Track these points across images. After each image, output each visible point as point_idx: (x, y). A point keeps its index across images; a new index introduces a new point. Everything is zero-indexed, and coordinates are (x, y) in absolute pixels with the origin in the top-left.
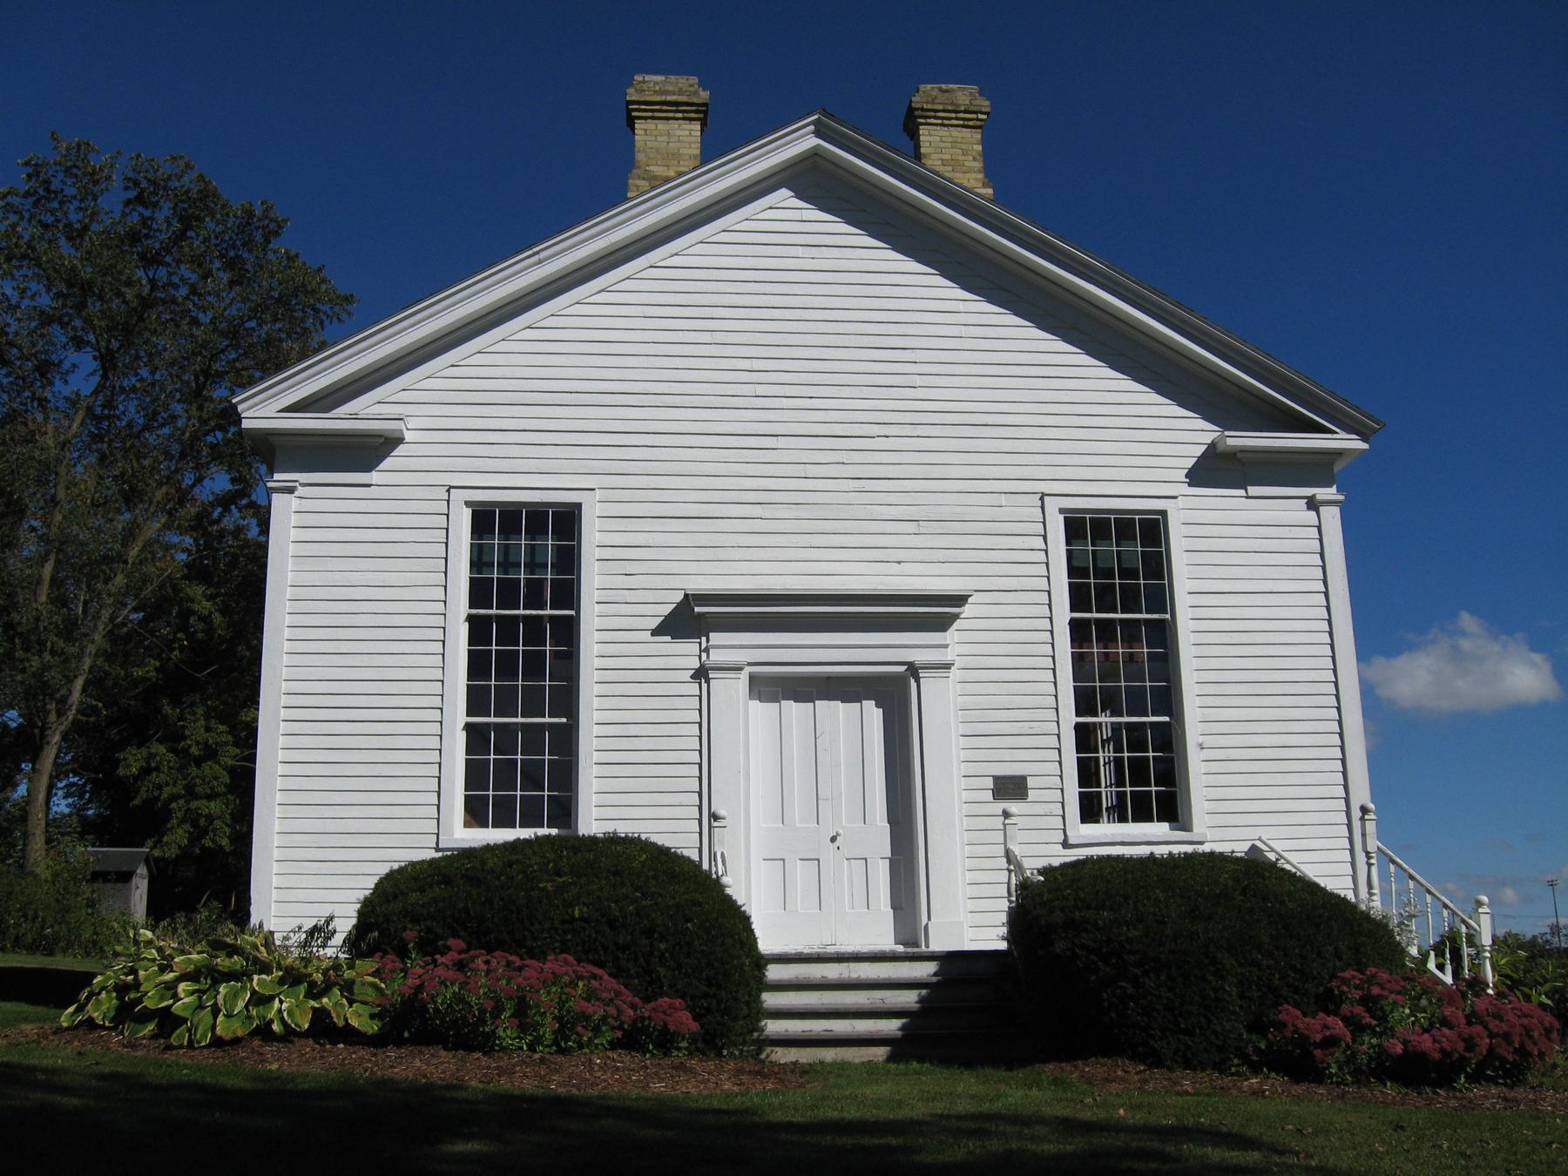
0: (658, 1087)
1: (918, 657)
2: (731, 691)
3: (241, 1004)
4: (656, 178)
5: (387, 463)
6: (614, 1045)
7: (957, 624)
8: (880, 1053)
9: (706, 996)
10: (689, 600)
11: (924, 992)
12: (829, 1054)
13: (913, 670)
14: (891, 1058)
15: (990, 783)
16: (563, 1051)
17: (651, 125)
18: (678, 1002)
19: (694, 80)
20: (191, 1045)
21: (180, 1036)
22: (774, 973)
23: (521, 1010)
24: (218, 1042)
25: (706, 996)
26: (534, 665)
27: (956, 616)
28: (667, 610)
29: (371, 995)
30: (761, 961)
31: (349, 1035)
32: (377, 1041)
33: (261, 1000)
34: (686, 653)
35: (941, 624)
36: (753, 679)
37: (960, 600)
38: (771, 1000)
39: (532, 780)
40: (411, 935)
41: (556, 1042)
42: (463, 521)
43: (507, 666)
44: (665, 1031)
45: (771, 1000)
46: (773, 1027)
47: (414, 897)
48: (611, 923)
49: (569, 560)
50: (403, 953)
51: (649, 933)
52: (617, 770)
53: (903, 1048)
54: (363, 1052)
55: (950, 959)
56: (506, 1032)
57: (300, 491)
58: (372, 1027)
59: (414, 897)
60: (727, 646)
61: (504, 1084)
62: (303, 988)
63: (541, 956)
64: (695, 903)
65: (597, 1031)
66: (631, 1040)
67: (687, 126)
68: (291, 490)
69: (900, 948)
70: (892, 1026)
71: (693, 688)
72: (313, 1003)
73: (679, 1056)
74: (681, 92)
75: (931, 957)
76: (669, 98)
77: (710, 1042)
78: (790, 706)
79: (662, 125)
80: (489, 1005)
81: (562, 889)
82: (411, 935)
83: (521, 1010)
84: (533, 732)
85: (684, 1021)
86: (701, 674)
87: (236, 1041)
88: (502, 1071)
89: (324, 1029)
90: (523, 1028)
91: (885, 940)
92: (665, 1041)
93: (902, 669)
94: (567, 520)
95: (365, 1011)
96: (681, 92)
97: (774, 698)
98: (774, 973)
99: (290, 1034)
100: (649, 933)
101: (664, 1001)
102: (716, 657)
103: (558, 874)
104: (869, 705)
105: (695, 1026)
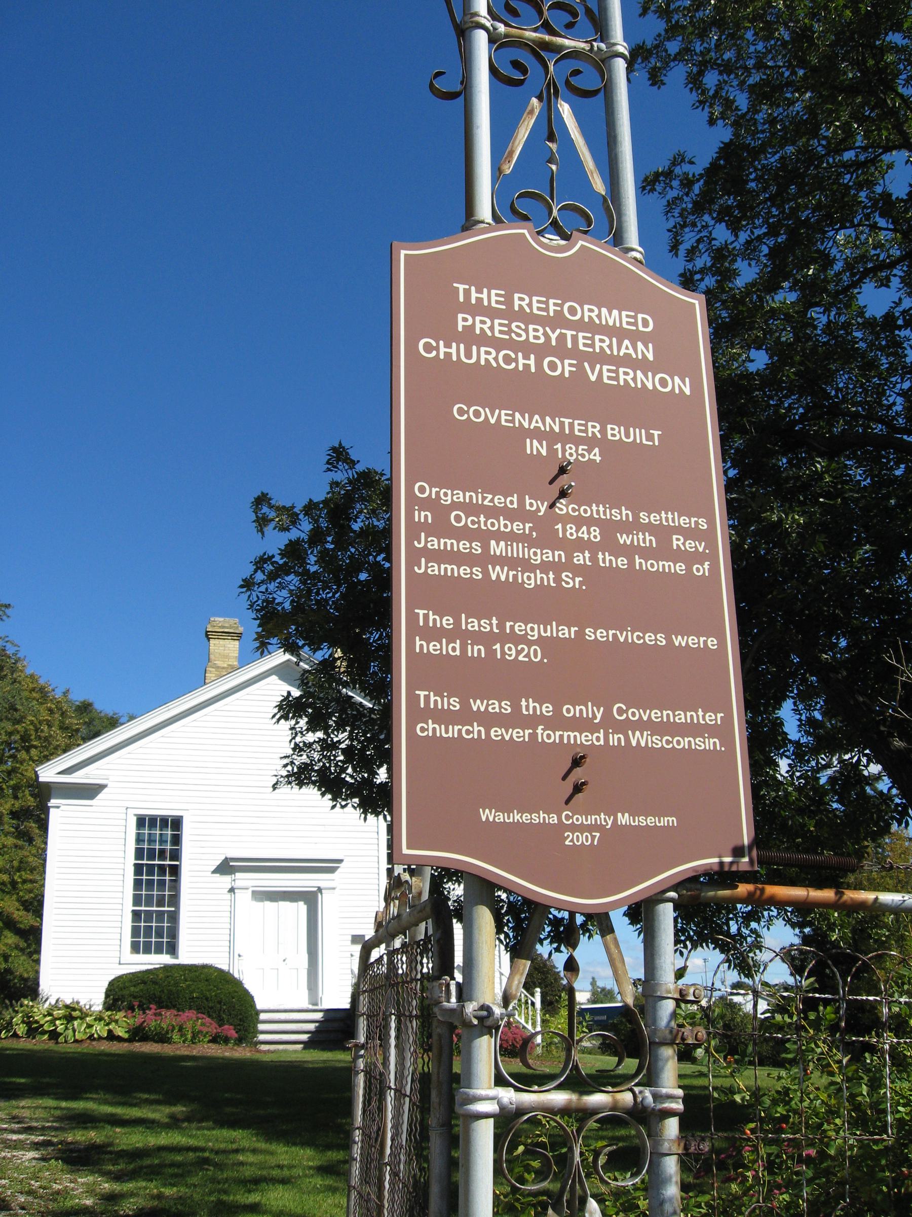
0: (227, 1054)
1: (322, 884)
2: (244, 898)
3: (83, 1028)
4: (218, 667)
5: (100, 796)
6: (210, 1041)
7: (339, 870)
8: (300, 1046)
9: (239, 1025)
10: (226, 861)
11: (317, 1024)
12: (281, 1047)
13: (320, 889)
14: (304, 1048)
15: (350, 938)
16: (193, 1043)
17: (217, 641)
18: (232, 1027)
19: (237, 620)
20: (66, 1042)
21: (61, 1039)
22: (263, 1016)
23: (181, 1029)
24: (76, 1041)
25: (239, 1025)
26: (162, 883)
27: (338, 867)
28: (218, 863)
29: (125, 1024)
30: (258, 1013)
31: (119, 1039)
32: (129, 1040)
33: (90, 1026)
34: (225, 881)
35: (332, 870)
36: (253, 892)
37: (340, 861)
38: (261, 1027)
39: (159, 934)
40: (136, 1004)
41: (192, 1040)
42: (133, 822)
43: (150, 883)
44: (226, 1037)
45: (261, 1027)
46: (262, 1037)
47: (132, 989)
48: (207, 999)
49: (177, 840)
50: (133, 1010)
51: (220, 1002)
52: (195, 931)
53: (308, 1045)
54: (126, 1044)
55: (327, 1011)
56: (176, 1037)
57: (62, 808)
58: (126, 1036)
59: (132, 989)
60: (242, 879)
61: (178, 1053)
62: (102, 1022)
63: (183, 1011)
64: (235, 992)
65: (205, 1036)
66: (214, 1040)
67: (233, 642)
68: (58, 807)
69: (311, 1007)
70: (305, 1037)
71: (228, 896)
72: (107, 1028)
73: (231, 1045)
74: (230, 627)
75: (321, 1011)
76: (226, 630)
77: (240, 1041)
78: (268, 904)
79: (222, 642)
80: (171, 1028)
81: (188, 986)
82: (136, 1004)
83: (181, 1029)
84: (160, 914)
85: (233, 1033)
86: (232, 890)
87: (82, 1041)
88: (177, 1049)
89: (111, 1036)
90: (182, 1036)
91: (306, 1005)
92: (226, 1040)
93: (315, 889)
94: (176, 823)
95: (123, 1030)
96: (230, 627)
97: (261, 900)
98: (263, 1016)
99: (100, 1038)
100: (220, 1002)
101: (226, 1026)
102: (238, 884)
103: (186, 981)
104: (301, 904)
105: (236, 1035)
